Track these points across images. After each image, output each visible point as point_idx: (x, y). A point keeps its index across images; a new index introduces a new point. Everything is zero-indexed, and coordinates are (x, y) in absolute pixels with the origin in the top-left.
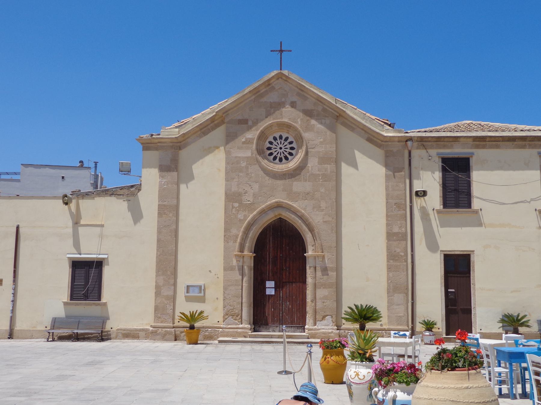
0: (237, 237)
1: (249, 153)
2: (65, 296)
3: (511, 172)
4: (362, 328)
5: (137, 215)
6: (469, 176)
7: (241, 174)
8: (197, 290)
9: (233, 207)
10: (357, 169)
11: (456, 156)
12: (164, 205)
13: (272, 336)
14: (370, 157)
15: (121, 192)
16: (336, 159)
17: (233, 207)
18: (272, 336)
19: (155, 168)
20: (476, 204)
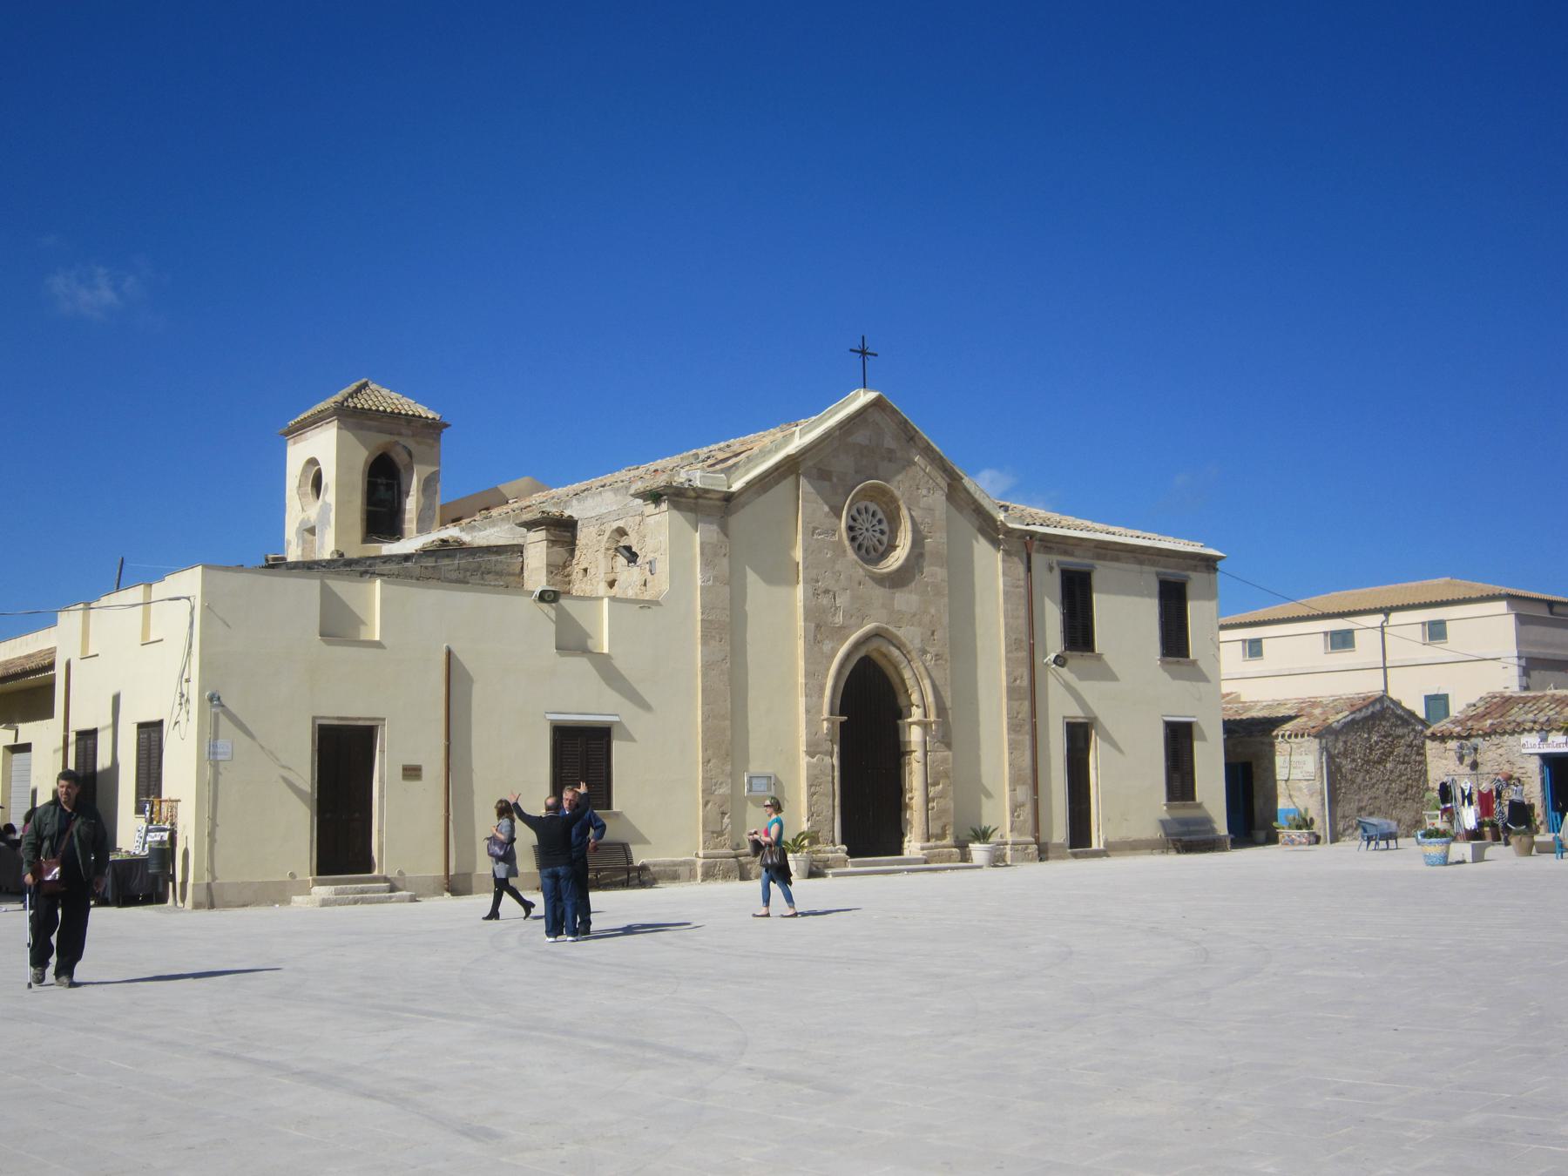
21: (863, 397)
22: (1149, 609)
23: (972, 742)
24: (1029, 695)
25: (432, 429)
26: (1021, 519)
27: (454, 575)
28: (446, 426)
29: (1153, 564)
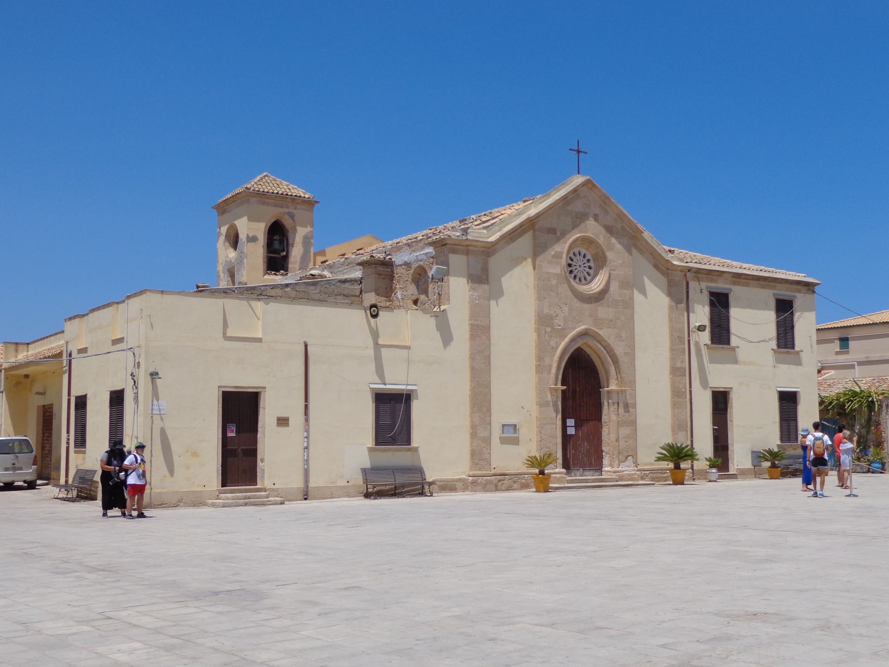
0: (550, 366)
1: (558, 269)
2: (370, 441)
3: (756, 311)
4: (677, 467)
5: (447, 338)
6: (728, 313)
7: (552, 294)
8: (512, 430)
9: (546, 332)
10: (646, 297)
11: (719, 291)
12: (477, 325)
13: (586, 481)
14: (656, 285)
15: (273, 292)
16: (633, 284)
17: (546, 332)
18: (586, 481)
19: (463, 277)
20: (734, 341)
21: (578, 180)
22: (769, 318)
23: (649, 402)
24: (680, 373)
25: (310, 204)
26: (681, 260)
27: (317, 297)
28: (317, 202)
29: (771, 288)
